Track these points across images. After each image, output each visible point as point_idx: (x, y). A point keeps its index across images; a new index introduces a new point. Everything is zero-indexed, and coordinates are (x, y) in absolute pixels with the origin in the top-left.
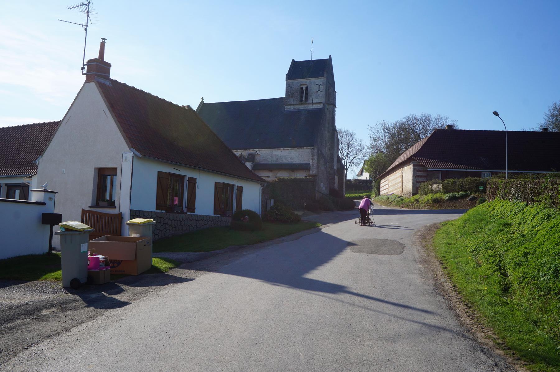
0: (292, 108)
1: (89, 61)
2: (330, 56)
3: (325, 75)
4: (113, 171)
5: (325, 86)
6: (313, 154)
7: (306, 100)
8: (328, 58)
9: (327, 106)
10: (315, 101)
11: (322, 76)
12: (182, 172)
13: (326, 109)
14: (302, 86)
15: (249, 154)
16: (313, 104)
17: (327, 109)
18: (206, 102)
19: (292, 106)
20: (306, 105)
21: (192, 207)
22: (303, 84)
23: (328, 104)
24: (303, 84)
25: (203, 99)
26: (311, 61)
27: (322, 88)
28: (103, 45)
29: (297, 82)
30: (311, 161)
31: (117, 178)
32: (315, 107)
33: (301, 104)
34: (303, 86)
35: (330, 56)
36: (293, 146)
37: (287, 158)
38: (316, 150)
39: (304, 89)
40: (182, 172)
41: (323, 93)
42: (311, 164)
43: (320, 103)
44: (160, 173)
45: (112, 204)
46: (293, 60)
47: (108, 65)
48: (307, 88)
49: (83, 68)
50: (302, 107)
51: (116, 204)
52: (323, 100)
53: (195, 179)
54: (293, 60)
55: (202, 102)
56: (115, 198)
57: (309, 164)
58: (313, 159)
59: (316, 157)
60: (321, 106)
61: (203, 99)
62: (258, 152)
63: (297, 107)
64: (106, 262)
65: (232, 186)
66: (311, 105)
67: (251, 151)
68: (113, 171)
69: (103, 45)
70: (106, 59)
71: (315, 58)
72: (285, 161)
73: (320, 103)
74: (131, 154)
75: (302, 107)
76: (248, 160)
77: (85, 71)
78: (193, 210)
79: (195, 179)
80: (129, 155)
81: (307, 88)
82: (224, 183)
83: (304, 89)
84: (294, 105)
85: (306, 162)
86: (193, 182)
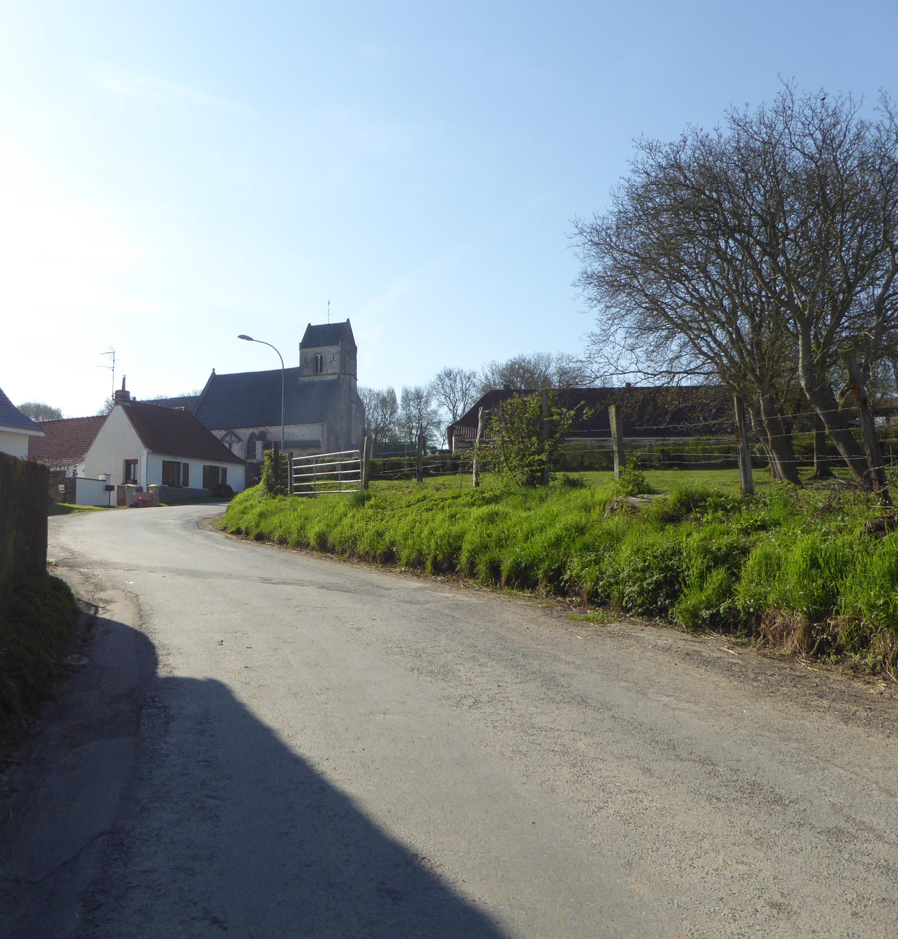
0: (306, 379)
1: (117, 392)
2: (348, 320)
3: (340, 343)
4: (135, 462)
5: (339, 355)
6: (323, 431)
7: (321, 370)
8: (345, 321)
9: (342, 376)
10: (330, 371)
11: (337, 344)
12: (178, 460)
13: (341, 380)
14: (317, 355)
15: (261, 432)
16: (328, 374)
17: (343, 379)
18: (217, 373)
19: (306, 378)
20: (320, 377)
21: (186, 483)
22: (317, 353)
23: (344, 374)
24: (317, 353)
25: (214, 370)
26: (329, 325)
27: (337, 357)
28: (124, 379)
29: (311, 351)
30: (321, 437)
31: (138, 466)
32: (331, 378)
33: (316, 375)
34: (317, 355)
35: (348, 320)
36: (303, 423)
37: (298, 435)
38: (325, 426)
39: (319, 358)
40: (178, 460)
41: (338, 362)
42: (321, 440)
43: (335, 374)
44: (164, 462)
45: (135, 482)
46: (309, 324)
47: (128, 392)
48: (321, 357)
49: (113, 396)
50: (317, 378)
51: (138, 482)
52: (337, 370)
53: (188, 464)
54: (309, 324)
55: (213, 373)
56: (137, 478)
57: (320, 441)
58: (323, 436)
59: (325, 434)
60: (335, 377)
61: (214, 370)
62: (269, 429)
63: (311, 378)
64: (141, 500)
65: (218, 468)
66: (326, 376)
67: (262, 429)
68: (135, 462)
69: (124, 379)
70: (126, 389)
71: (331, 323)
72: (296, 439)
73: (335, 374)
74: (146, 451)
75: (317, 378)
76: (258, 439)
77: (114, 398)
78: (187, 485)
79: (188, 464)
80: (145, 452)
81: (321, 357)
82: (210, 466)
83: (319, 358)
84: (308, 376)
85: (317, 439)
86: (186, 466)
